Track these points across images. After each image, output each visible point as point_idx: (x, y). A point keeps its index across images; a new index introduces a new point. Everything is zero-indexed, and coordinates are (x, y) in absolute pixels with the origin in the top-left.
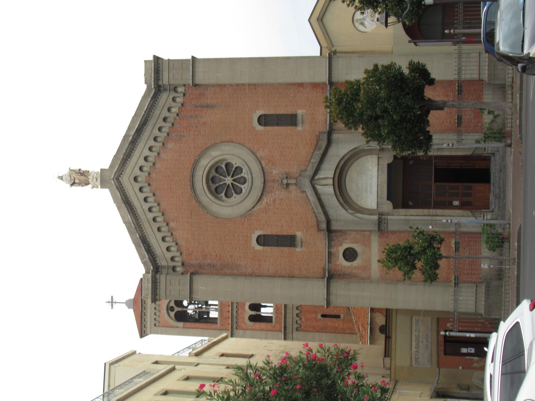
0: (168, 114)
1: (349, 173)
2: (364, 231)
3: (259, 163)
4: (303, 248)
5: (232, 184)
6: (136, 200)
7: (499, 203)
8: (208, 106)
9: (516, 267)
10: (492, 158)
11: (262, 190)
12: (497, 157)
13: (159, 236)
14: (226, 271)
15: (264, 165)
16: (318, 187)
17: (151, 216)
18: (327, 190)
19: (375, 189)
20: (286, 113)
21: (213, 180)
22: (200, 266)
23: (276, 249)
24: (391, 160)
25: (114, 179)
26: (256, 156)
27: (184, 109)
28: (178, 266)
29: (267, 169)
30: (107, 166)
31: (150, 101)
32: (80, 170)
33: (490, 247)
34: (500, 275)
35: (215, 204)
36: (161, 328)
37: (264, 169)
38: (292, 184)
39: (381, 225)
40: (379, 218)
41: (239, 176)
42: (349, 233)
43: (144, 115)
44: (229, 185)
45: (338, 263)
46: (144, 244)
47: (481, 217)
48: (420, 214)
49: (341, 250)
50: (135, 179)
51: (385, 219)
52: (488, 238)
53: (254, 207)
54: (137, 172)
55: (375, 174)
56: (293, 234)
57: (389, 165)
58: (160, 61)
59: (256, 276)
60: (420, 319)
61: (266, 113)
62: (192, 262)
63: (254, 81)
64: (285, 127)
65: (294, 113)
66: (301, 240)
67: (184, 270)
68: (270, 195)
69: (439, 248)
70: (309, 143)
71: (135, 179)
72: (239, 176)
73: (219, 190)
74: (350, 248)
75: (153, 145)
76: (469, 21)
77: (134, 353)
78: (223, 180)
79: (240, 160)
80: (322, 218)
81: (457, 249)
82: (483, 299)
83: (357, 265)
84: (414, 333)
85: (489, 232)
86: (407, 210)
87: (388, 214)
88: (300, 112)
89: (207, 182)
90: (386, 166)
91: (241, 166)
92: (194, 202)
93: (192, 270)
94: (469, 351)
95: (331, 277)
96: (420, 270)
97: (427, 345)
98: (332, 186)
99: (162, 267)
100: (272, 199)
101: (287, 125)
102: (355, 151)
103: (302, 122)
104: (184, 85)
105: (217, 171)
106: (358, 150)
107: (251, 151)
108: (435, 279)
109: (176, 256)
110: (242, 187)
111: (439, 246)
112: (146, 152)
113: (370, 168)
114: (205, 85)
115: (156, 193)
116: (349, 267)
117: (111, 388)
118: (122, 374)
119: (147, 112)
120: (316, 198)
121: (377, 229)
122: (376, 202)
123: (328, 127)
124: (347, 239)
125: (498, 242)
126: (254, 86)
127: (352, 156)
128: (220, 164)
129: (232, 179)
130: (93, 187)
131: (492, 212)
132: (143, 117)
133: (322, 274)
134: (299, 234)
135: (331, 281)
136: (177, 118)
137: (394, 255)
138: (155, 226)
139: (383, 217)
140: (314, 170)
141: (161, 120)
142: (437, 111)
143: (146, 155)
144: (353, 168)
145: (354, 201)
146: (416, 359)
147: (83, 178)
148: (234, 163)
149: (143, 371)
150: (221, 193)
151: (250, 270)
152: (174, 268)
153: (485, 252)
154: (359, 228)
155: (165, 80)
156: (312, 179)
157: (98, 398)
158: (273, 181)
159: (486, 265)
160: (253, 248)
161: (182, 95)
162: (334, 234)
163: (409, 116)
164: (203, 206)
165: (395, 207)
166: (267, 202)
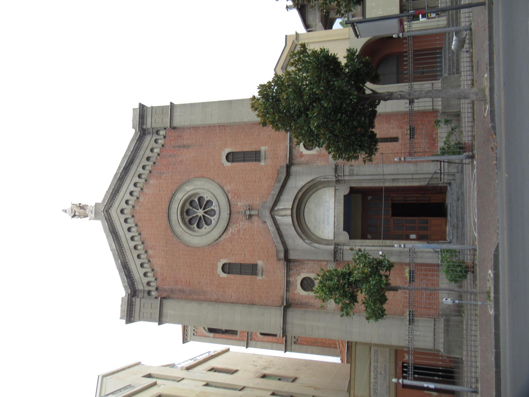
0: (150, 154)
1: (307, 205)
2: (321, 261)
3: (226, 196)
4: (264, 277)
5: (204, 216)
6: (121, 228)
7: (457, 232)
8: (184, 146)
9: (492, 304)
10: (449, 188)
11: (228, 221)
12: (454, 186)
13: (139, 262)
15: (230, 198)
16: (277, 217)
17: (132, 244)
18: (286, 220)
20: (250, 150)
22: (172, 291)
23: (238, 277)
24: (347, 192)
25: (105, 212)
26: (224, 190)
27: (164, 150)
28: (153, 291)
29: (233, 201)
30: (100, 201)
31: (136, 143)
32: (80, 204)
33: (451, 277)
34: (459, 311)
35: (187, 234)
36: (197, 336)
37: (230, 201)
40: (335, 248)
41: (210, 209)
42: (306, 262)
44: (200, 217)
45: (296, 292)
46: (125, 269)
48: (376, 244)
49: (299, 279)
50: (122, 211)
51: (341, 249)
52: (449, 267)
53: (220, 237)
55: (332, 205)
56: (255, 263)
57: (345, 196)
58: (145, 108)
59: (220, 302)
60: (379, 350)
61: (234, 150)
63: (222, 121)
65: (258, 150)
66: (262, 269)
67: (158, 294)
69: (387, 277)
71: (122, 211)
72: (210, 209)
73: (193, 221)
74: (308, 277)
75: (137, 181)
76: (421, 70)
77: (139, 364)
78: (196, 213)
79: (210, 194)
80: (281, 248)
81: (412, 279)
82: (442, 335)
84: (373, 364)
85: (449, 260)
86: (363, 241)
87: (344, 245)
88: (263, 149)
89: (182, 214)
90: (342, 197)
91: (212, 199)
92: (169, 231)
93: (164, 295)
95: (288, 306)
96: (364, 303)
98: (290, 217)
99: (139, 291)
100: (236, 229)
101: (252, 161)
102: (312, 183)
103: (265, 158)
104: (165, 129)
105: (191, 203)
106: (315, 182)
107: (220, 185)
108: (383, 316)
109: (152, 281)
110: (212, 218)
111: (387, 273)
112: (132, 188)
113: (328, 199)
115: (139, 224)
116: (306, 296)
118: (112, 385)
120: (275, 228)
121: (332, 259)
122: (333, 233)
123: (288, 161)
124: (304, 269)
125: (461, 271)
126: (222, 127)
127: (309, 188)
130: (90, 219)
133: (280, 303)
134: (260, 263)
135: (288, 309)
136: (159, 157)
137: (328, 283)
139: (339, 247)
140: (273, 202)
141: (144, 159)
143: (132, 190)
144: (311, 200)
145: (312, 231)
146: (375, 390)
147: (82, 211)
148: (205, 197)
149: (128, 384)
151: (215, 297)
152: (149, 293)
153: (444, 281)
154: (315, 258)
155: (148, 125)
156: (272, 209)
158: (238, 213)
159: (449, 299)
160: (219, 275)
161: (163, 137)
162: (292, 264)
163: (344, 106)
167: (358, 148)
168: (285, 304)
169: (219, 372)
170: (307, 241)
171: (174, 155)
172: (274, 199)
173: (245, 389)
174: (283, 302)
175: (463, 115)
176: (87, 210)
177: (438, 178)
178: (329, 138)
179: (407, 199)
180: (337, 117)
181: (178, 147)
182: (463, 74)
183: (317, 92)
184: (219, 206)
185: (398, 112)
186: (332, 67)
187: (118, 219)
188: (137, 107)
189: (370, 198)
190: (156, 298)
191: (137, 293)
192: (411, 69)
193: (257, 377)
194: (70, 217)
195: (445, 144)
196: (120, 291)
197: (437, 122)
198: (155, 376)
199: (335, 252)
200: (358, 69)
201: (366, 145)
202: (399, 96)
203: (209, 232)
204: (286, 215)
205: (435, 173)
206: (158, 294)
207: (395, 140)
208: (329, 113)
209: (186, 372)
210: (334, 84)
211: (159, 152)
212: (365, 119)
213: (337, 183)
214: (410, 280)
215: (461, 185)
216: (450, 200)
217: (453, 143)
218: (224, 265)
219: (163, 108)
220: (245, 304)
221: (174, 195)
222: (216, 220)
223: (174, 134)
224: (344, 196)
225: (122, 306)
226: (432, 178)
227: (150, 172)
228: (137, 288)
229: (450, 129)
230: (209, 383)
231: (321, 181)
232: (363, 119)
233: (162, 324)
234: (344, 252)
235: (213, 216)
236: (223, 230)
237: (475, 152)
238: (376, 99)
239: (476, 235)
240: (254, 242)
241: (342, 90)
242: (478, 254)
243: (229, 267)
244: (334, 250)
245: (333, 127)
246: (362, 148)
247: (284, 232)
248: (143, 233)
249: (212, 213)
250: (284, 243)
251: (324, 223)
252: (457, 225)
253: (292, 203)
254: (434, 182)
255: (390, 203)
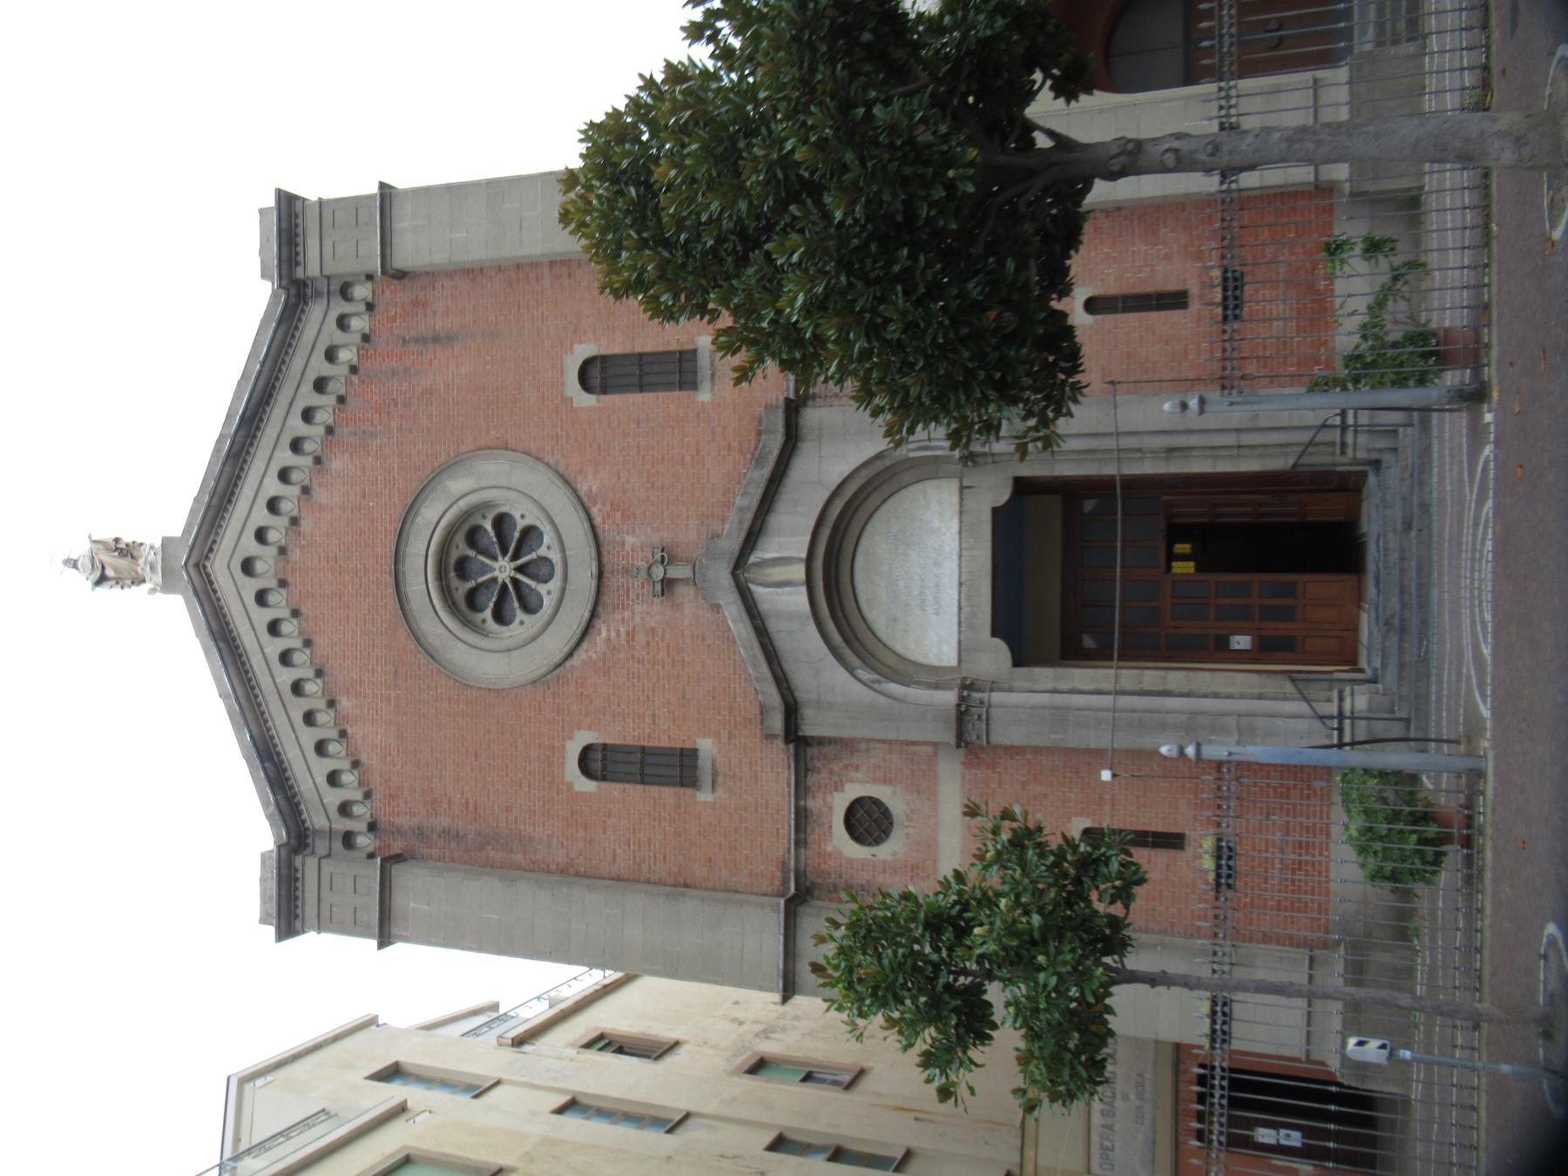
0: (326, 369)
1: (864, 542)
2: (913, 743)
3: (582, 515)
4: (720, 792)
5: (515, 582)
6: (248, 624)
7: (1401, 650)
8: (436, 339)
10: (1372, 479)
11: (592, 600)
12: (1393, 474)
13: (309, 737)
14: (491, 854)
15: (598, 520)
16: (757, 590)
17: (286, 676)
18: (787, 600)
19: (950, 595)
20: (661, 349)
21: (462, 568)
22: (420, 833)
23: (635, 792)
24: (1003, 496)
25: (194, 566)
26: (575, 491)
29: (606, 529)
30: (176, 531)
32: (117, 540)
35: (460, 644)
37: (600, 533)
38: (685, 581)
39: (967, 726)
40: (962, 699)
42: (863, 746)
43: (260, 372)
44: (504, 586)
45: (829, 848)
46: (267, 758)
47: (1329, 700)
49: (840, 803)
50: (248, 567)
51: (982, 702)
53: (570, 655)
54: (250, 546)
56: (688, 745)
57: (995, 511)
58: (298, 204)
59: (577, 875)
61: (604, 352)
62: (398, 821)
64: (661, 394)
67: (378, 843)
68: (618, 616)
70: (735, 444)
71: (248, 567)
72: (533, 556)
74: (871, 798)
75: (288, 464)
77: (372, 1022)
78: (486, 569)
80: (774, 699)
83: (890, 858)
87: (994, 687)
89: (441, 575)
90: (987, 517)
91: (538, 524)
92: (403, 633)
93: (396, 848)
94: (1283, 1142)
97: (1139, 1108)
98: (804, 589)
99: (316, 832)
101: (667, 386)
102: (879, 466)
103: (713, 376)
106: (888, 462)
107: (561, 476)
110: (542, 589)
111: (1117, 909)
112: (273, 487)
113: (936, 523)
114: (427, 273)
115: (303, 610)
116: (864, 864)
117: (244, 1146)
118: (273, 1109)
119: (269, 363)
120: (750, 629)
121: (952, 739)
122: (955, 644)
124: (857, 768)
127: (868, 483)
128: (476, 520)
129: (513, 565)
130: (153, 591)
131: (1374, 681)
132: (257, 378)
133: (777, 883)
135: (802, 909)
136: (355, 379)
138: (298, 707)
140: (743, 534)
141: (307, 387)
142: (1163, 313)
143: (273, 493)
144: (876, 524)
147: (124, 563)
148: (517, 515)
150: (482, 610)
151: (560, 857)
152: (348, 839)
154: (892, 735)
155: (312, 267)
156: (740, 563)
157: (539, 998)
158: (627, 571)
160: (570, 785)
161: (362, 307)
162: (813, 751)
164: (426, 651)
165: (1018, 662)
166: (609, 639)
167: (992, 394)
168: (792, 890)
169: (620, 1050)
170: (861, 673)
171: (406, 370)
172: (746, 526)
173: (690, 1122)
174: (785, 882)
175: (1432, 202)
176: (141, 561)
177: (1333, 444)
178: (866, 354)
179: (1219, 510)
180: (890, 262)
181: (417, 340)
182: (1434, 43)
183: (797, 156)
184: (563, 550)
185: (1187, 195)
186: (867, 37)
187: (235, 593)
188: (271, 202)
189: (1089, 505)
190: (371, 856)
191: (310, 841)
192: (1229, 30)
193: (735, 1072)
194: (89, 584)
195: (1364, 337)
196: (258, 835)
197: (1335, 249)
198: (412, 1070)
199: (962, 715)
200: (984, 43)
201: (1027, 381)
202: (1170, 159)
203: (534, 638)
204: (787, 583)
205: (1324, 426)
206: (378, 843)
207: (1175, 300)
208: (856, 249)
209: (510, 1054)
210: (869, 115)
211: (355, 361)
212: (1022, 266)
213: (966, 466)
214: (1218, 885)
215: (1420, 474)
216: (1378, 522)
217: (1395, 335)
218: (586, 752)
219: (356, 203)
220: (660, 883)
221: (411, 510)
222: (555, 595)
223: (401, 295)
224: (995, 511)
225: (263, 880)
226: (1311, 443)
227: (330, 430)
228: (308, 824)
229: (1386, 278)
230: (581, 1099)
231: (908, 459)
232: (1010, 264)
233: (390, 943)
234: (993, 712)
235: (546, 581)
236: (579, 632)
237: (1491, 373)
238: (1074, 168)
239: (1486, 713)
240: (683, 672)
241: (911, 141)
242: (1490, 792)
243: (604, 758)
244: (959, 706)
245: (874, 311)
246: (1008, 393)
247: (783, 642)
248: (317, 639)
249: (540, 570)
250: (782, 681)
251: (922, 605)
252: (1402, 620)
253: (808, 538)
254: (1319, 459)
255: (1163, 526)
